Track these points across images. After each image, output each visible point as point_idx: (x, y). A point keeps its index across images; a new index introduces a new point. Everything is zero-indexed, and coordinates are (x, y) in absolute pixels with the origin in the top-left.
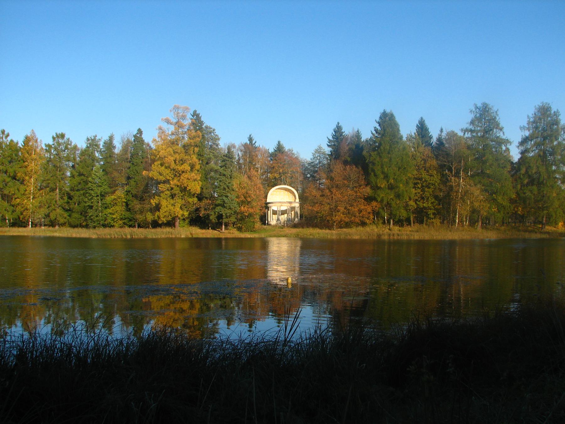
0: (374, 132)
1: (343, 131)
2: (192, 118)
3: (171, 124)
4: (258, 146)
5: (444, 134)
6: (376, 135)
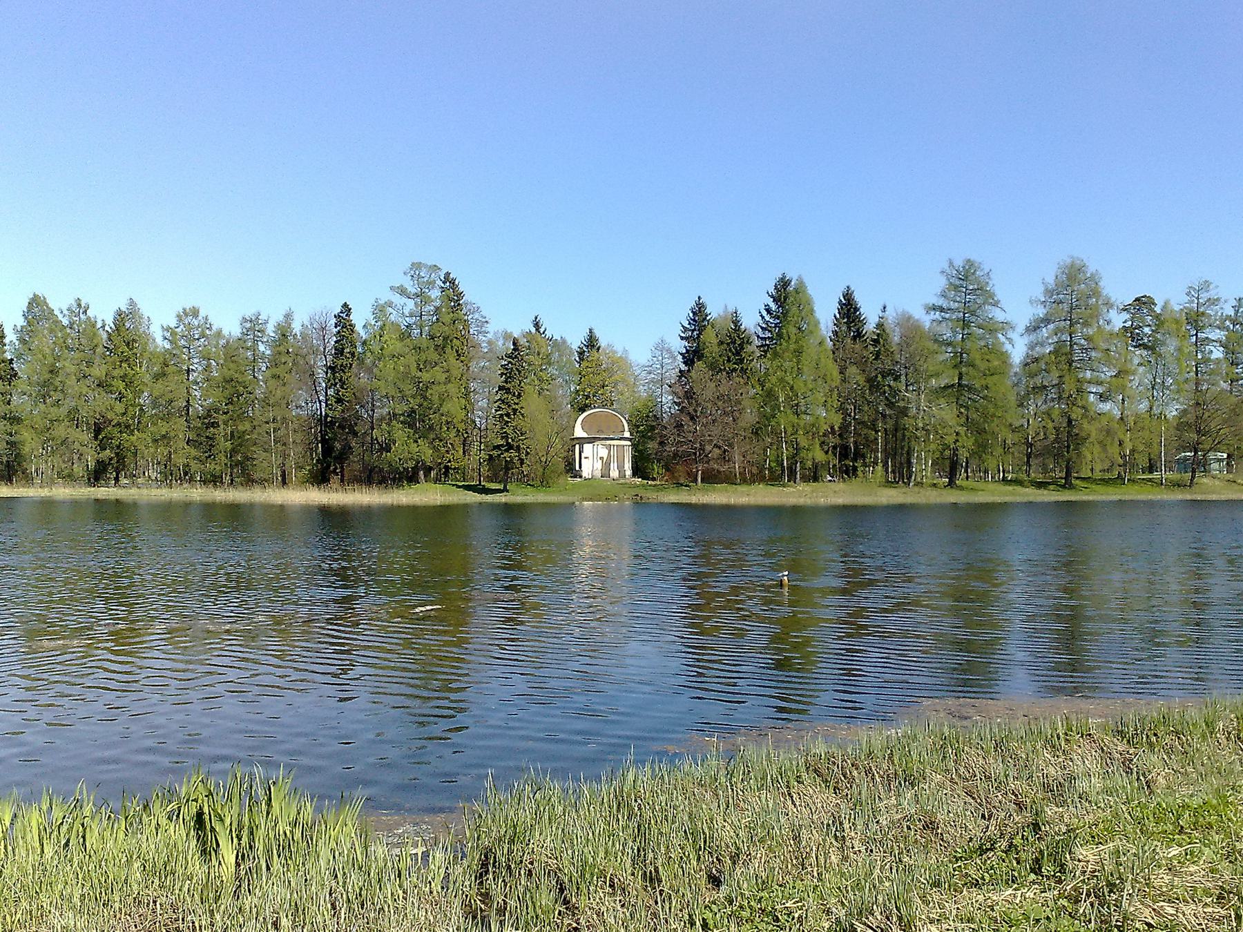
0: (764, 313)
1: (708, 311)
2: (443, 285)
5: (891, 315)
6: (767, 318)
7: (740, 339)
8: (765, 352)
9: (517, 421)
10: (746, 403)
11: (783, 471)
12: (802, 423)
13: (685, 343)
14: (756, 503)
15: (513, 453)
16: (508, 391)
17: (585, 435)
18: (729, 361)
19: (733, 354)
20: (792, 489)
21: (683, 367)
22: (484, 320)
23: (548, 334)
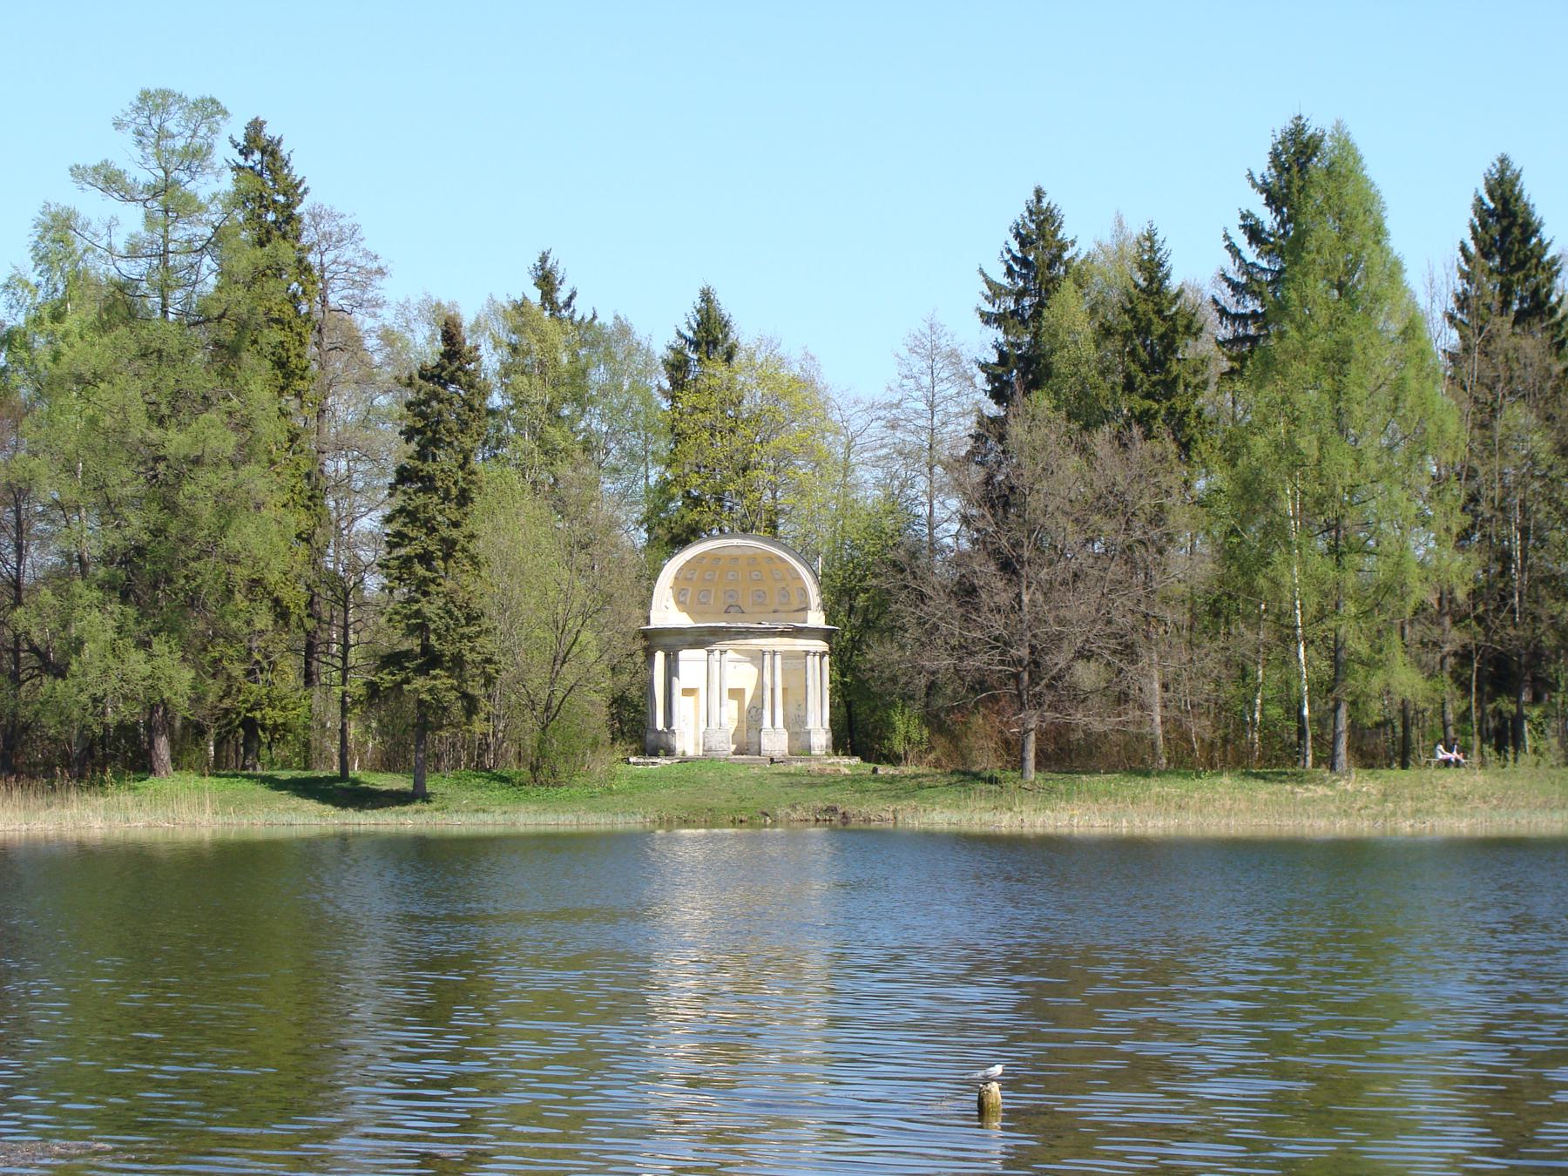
0: (1241, 240)
1: (1066, 233)
2: (241, 160)
3: (128, 195)
4: (589, 317)
6: (1250, 254)
7: (1164, 319)
8: (1242, 359)
9: (456, 580)
10: (1179, 516)
11: (1301, 733)
12: (1351, 580)
13: (997, 334)
14: (1330, 836)
15: (442, 680)
16: (428, 482)
17: (682, 620)
18: (1129, 386)
19: (1144, 368)
20: (1321, 790)
21: (992, 409)
22: (375, 266)
23: (582, 309)
